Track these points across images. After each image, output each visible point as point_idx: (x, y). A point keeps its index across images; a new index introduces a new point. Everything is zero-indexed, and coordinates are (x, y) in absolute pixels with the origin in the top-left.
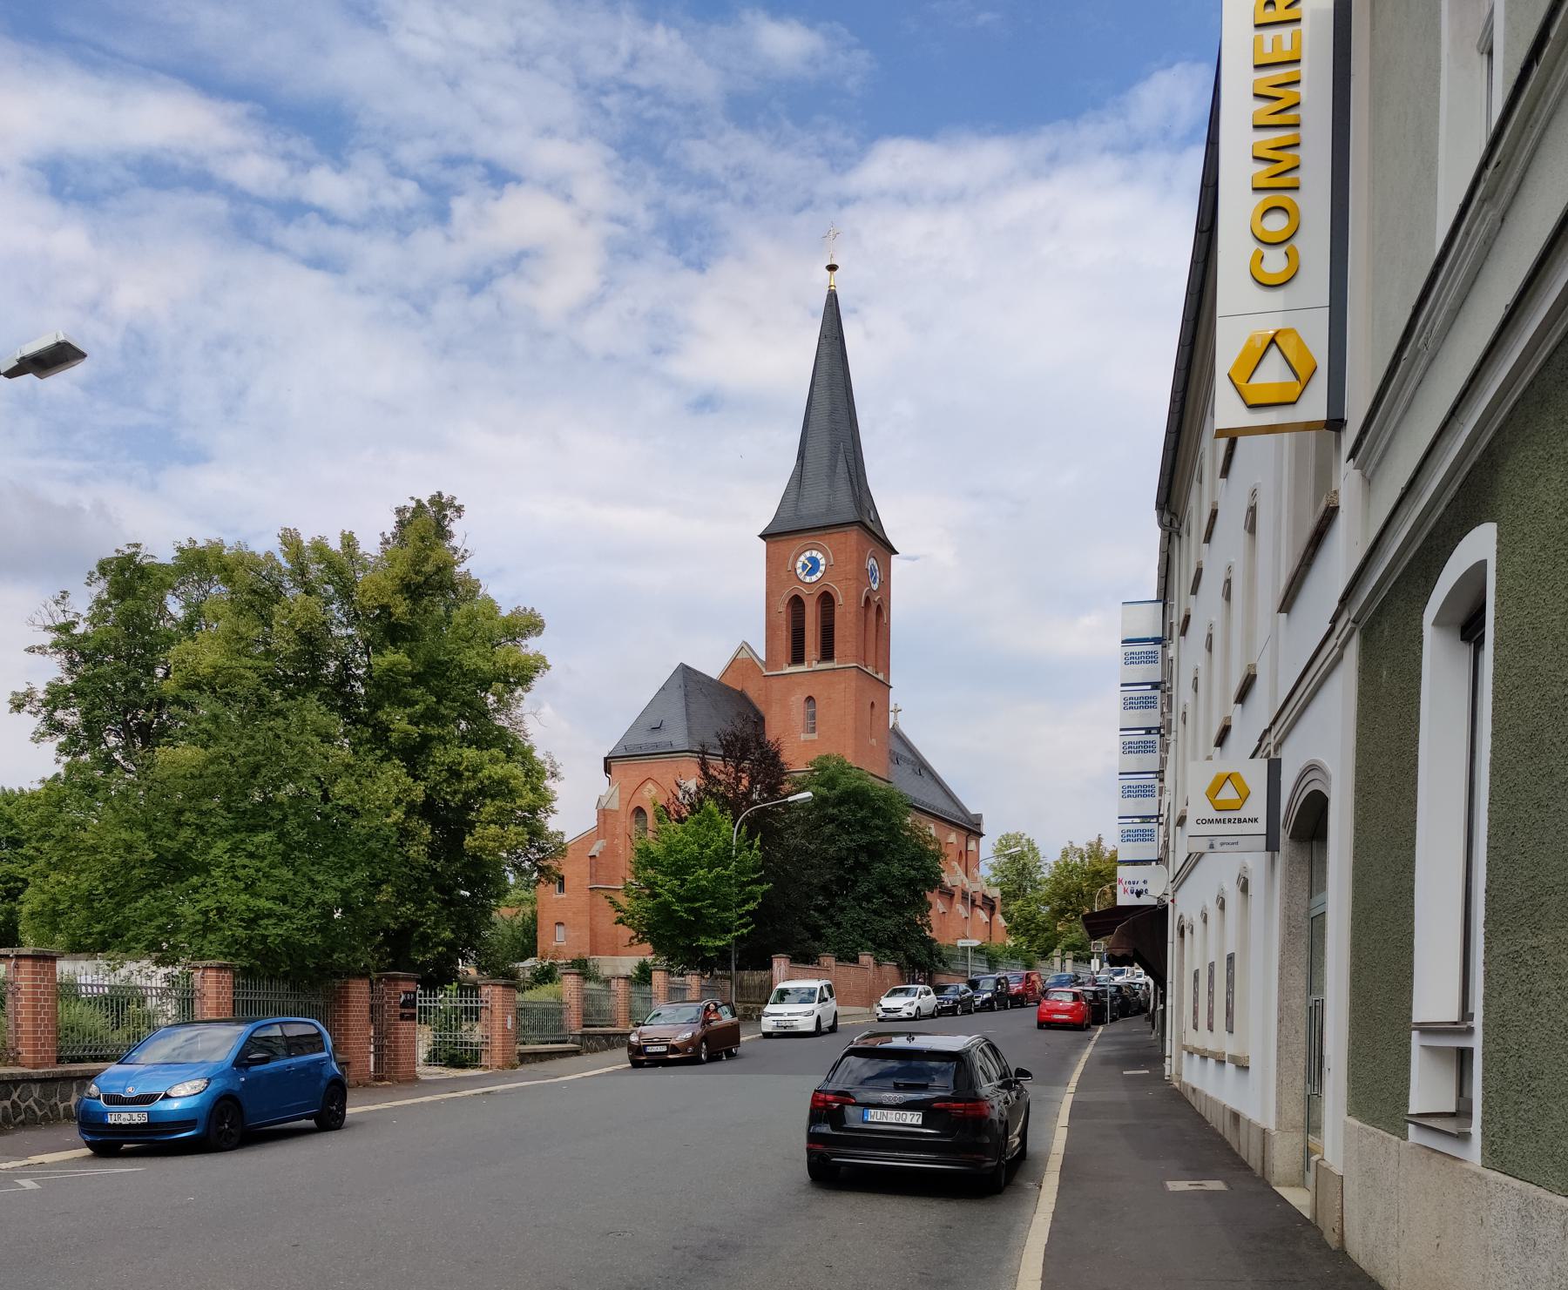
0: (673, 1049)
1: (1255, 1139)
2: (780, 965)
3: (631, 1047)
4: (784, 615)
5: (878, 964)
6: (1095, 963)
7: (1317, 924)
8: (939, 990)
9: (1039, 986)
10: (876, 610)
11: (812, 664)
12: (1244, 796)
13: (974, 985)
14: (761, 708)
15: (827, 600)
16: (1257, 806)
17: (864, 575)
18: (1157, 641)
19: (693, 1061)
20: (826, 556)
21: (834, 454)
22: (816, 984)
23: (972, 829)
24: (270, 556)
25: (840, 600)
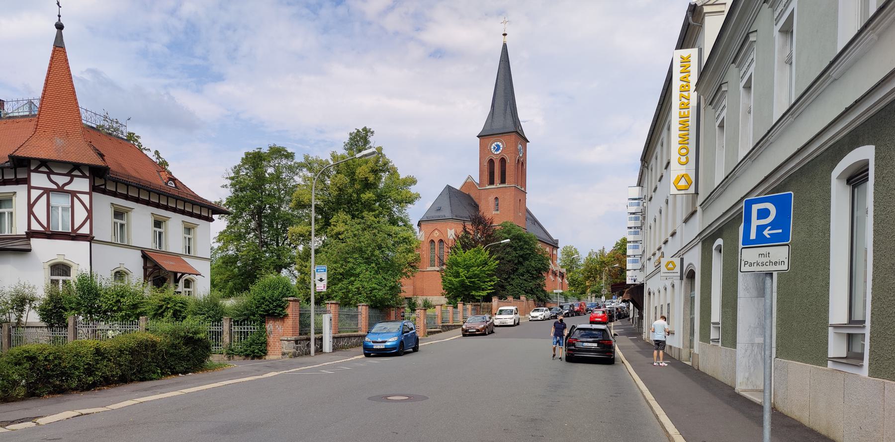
0: (478, 330)
1: (677, 352)
2: (495, 301)
3: (463, 330)
5: (527, 300)
6: (603, 298)
7: (693, 299)
8: (550, 309)
9: (585, 308)
10: (521, 164)
11: (497, 185)
12: (675, 267)
13: (562, 307)
14: (477, 201)
15: (503, 161)
16: (678, 269)
17: (517, 151)
18: (639, 199)
19: (484, 334)
20: (500, 141)
21: (506, 105)
22: (513, 308)
23: (554, 245)
24: (327, 161)
25: (508, 161)
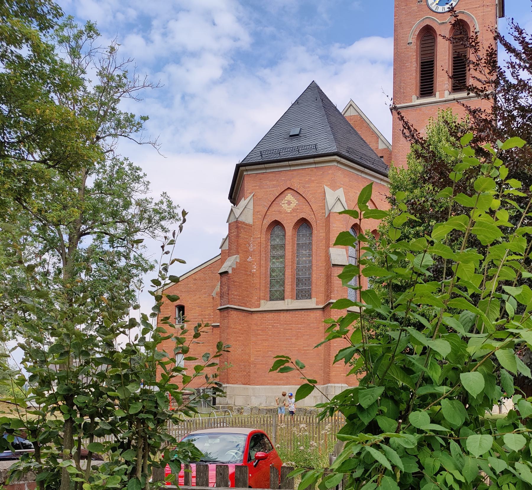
4: (414, 47)
